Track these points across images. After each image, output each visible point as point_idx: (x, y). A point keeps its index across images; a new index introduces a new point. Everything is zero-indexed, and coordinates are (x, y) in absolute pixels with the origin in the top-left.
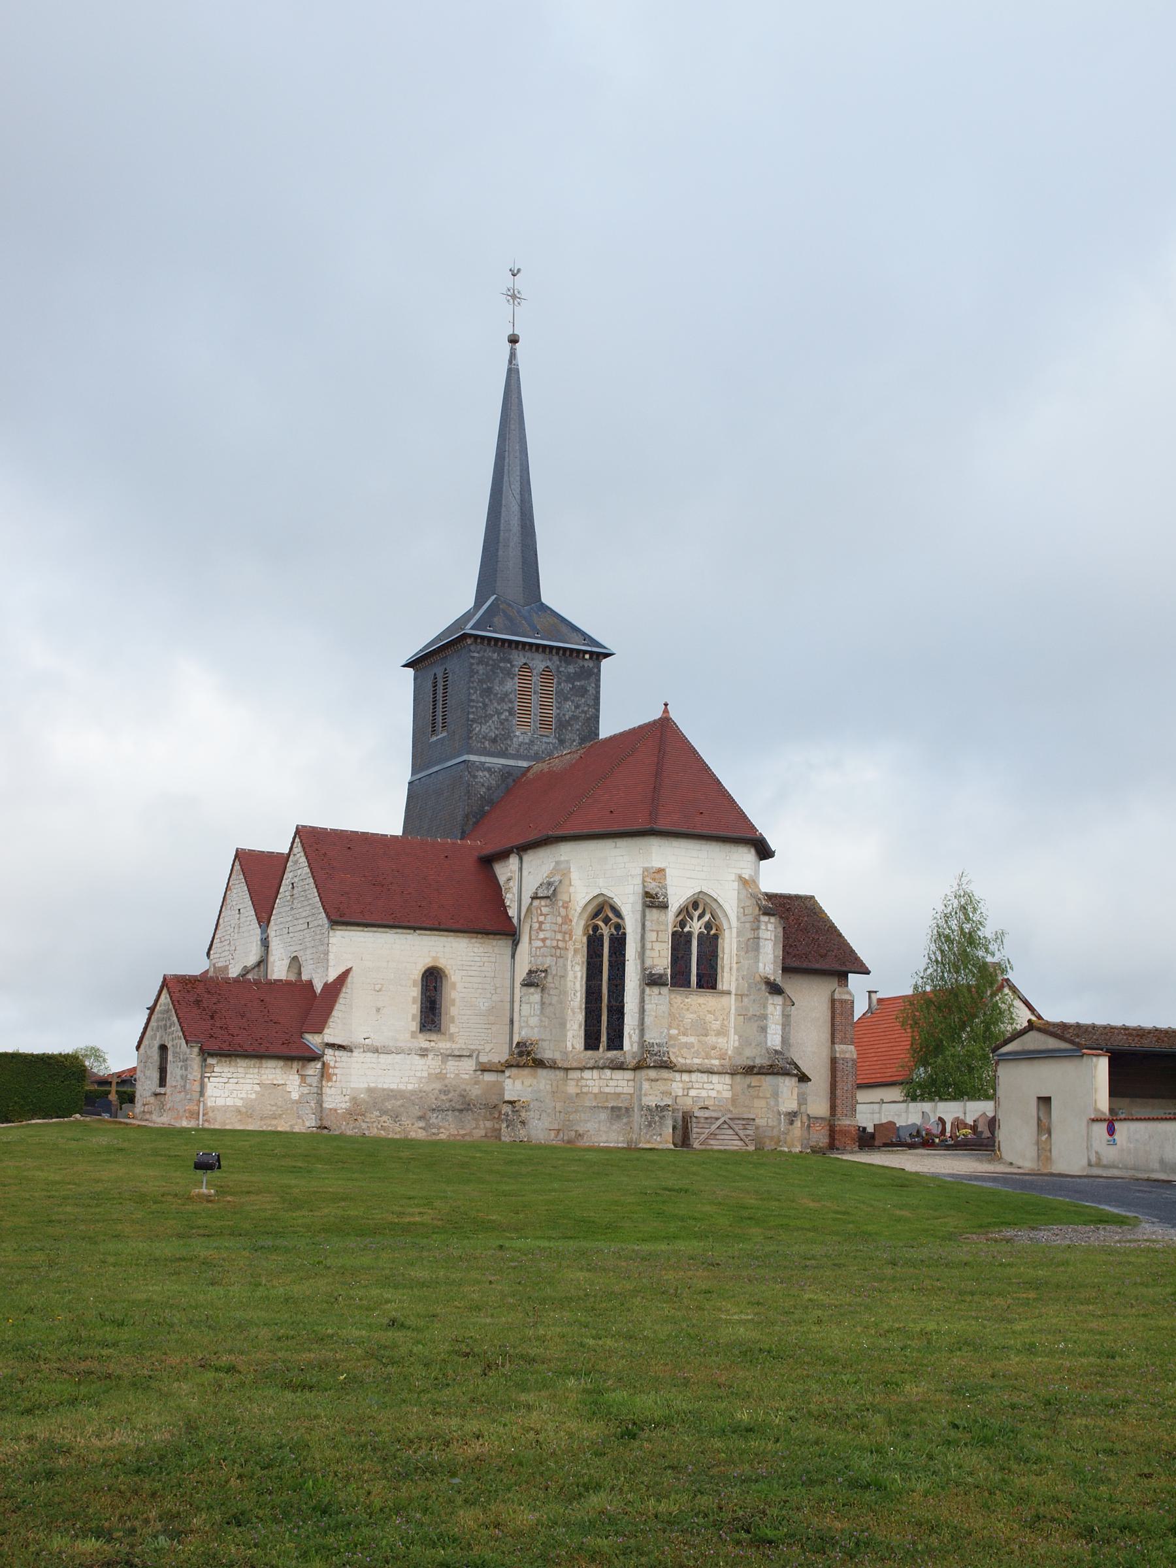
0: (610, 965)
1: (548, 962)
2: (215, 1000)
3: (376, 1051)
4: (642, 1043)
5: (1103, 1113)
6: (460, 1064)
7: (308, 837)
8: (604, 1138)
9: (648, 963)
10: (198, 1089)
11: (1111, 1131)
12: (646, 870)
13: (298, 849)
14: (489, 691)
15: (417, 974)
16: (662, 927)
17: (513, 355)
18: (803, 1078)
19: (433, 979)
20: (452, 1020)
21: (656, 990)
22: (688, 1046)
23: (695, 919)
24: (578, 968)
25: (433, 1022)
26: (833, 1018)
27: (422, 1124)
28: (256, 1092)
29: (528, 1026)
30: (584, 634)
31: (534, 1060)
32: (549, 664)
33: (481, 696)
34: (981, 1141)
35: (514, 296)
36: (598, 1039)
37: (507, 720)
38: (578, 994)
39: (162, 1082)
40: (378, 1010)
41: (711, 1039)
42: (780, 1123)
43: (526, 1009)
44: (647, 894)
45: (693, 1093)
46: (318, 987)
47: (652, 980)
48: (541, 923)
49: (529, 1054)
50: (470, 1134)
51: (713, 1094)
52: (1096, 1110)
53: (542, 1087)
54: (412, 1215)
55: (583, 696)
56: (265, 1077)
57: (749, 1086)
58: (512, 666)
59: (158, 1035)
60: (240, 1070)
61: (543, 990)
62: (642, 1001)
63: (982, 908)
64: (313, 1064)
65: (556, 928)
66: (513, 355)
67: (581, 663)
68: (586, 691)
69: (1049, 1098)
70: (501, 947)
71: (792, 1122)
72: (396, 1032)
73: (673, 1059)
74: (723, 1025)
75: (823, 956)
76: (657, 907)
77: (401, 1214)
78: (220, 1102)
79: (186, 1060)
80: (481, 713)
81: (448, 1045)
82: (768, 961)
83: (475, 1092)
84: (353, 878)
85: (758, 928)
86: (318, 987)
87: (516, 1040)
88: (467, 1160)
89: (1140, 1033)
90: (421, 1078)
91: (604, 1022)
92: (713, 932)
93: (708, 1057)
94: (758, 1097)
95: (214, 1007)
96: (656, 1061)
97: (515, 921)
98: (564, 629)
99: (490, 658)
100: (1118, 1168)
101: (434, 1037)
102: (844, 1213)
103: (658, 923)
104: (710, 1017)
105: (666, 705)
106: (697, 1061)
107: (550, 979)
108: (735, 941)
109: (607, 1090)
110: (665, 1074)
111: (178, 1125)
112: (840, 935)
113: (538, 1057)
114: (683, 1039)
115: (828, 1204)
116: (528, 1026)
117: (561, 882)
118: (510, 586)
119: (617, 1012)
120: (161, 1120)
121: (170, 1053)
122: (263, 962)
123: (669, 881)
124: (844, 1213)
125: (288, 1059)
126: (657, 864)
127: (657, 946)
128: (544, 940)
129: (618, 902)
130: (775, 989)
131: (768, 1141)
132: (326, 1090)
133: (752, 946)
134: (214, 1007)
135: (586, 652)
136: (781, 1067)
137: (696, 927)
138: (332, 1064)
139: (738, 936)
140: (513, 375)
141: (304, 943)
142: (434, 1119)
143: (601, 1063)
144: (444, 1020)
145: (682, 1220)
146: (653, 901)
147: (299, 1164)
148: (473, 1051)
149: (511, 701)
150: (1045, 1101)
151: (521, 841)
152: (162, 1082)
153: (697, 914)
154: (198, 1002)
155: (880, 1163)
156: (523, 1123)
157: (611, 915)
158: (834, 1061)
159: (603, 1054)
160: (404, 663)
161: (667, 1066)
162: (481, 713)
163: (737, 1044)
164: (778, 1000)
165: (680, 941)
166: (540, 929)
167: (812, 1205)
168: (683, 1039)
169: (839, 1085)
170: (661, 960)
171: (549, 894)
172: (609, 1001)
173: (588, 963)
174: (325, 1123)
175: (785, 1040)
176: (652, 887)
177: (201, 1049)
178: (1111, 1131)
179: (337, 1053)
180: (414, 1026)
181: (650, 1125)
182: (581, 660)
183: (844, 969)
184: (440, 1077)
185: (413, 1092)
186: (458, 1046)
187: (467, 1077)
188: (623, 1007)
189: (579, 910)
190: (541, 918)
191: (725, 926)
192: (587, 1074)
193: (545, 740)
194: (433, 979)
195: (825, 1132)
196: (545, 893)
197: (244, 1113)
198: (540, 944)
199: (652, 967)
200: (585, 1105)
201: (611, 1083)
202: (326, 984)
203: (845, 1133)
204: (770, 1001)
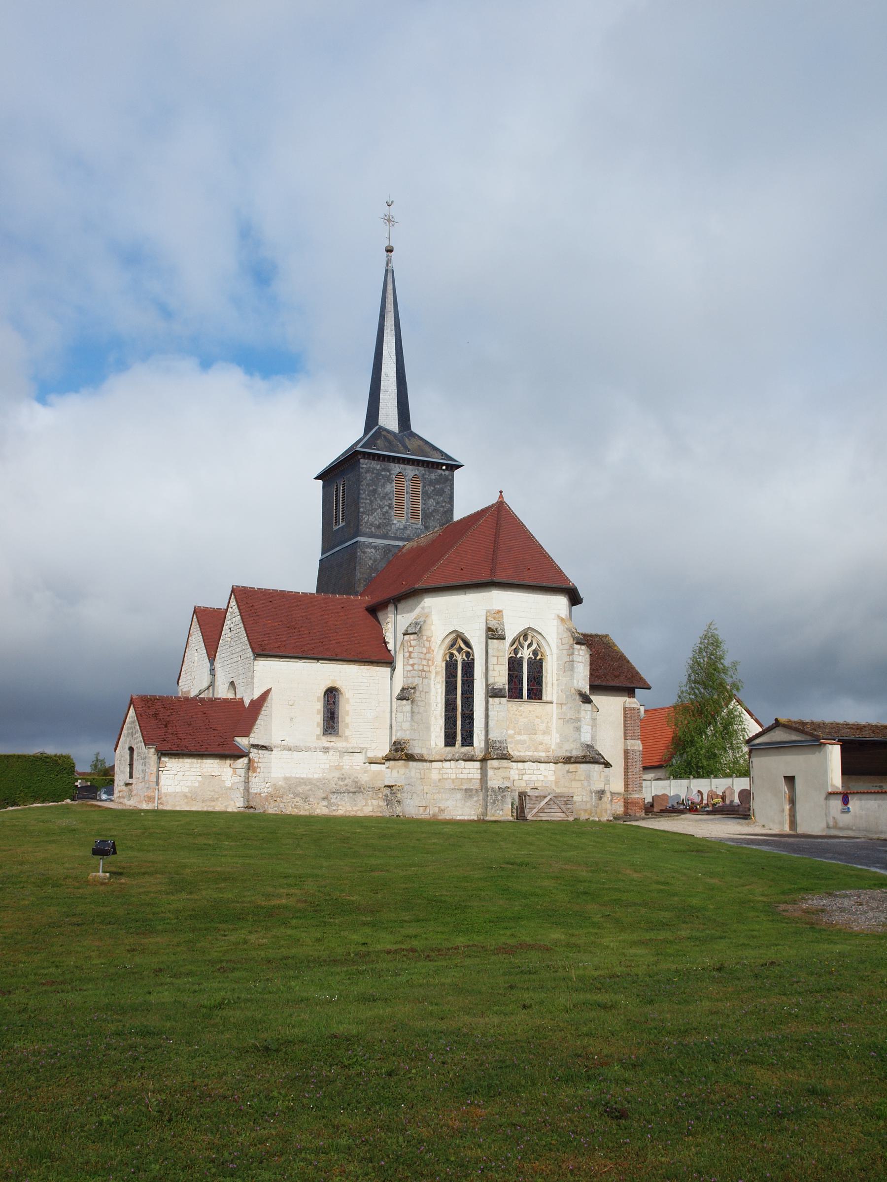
0: (463, 684)
1: (417, 681)
2: (169, 713)
3: (290, 750)
4: (487, 740)
5: (837, 788)
6: (353, 758)
7: (244, 596)
8: (460, 812)
9: (491, 681)
10: (155, 780)
11: (846, 802)
12: (488, 611)
13: (233, 603)
14: (375, 491)
15: (321, 692)
16: (501, 654)
17: (389, 261)
18: (607, 765)
19: (332, 695)
20: (347, 726)
21: (497, 700)
22: (523, 742)
23: (526, 647)
24: (438, 686)
25: (333, 728)
26: (625, 721)
27: (325, 803)
28: (199, 782)
29: (402, 729)
30: (441, 452)
31: (406, 755)
32: (417, 472)
33: (369, 495)
34: (740, 810)
35: (389, 220)
36: (455, 738)
37: (387, 512)
38: (439, 705)
39: (131, 777)
40: (291, 719)
41: (539, 737)
42: (592, 799)
43: (400, 715)
44: (489, 629)
45: (526, 777)
46: (247, 703)
47: (493, 693)
48: (410, 653)
49: (402, 750)
50: (361, 810)
51: (541, 778)
52: (833, 786)
53: (413, 774)
54: (280, 896)
55: (441, 495)
56: (205, 770)
57: (568, 772)
58: (391, 474)
59: (128, 740)
60: (186, 765)
61: (412, 702)
62: (487, 709)
63: (724, 647)
64: (241, 760)
65: (422, 656)
66: (389, 261)
67: (440, 472)
68: (444, 492)
69: (794, 777)
70: (383, 672)
71: (600, 798)
72: (324, 744)
73: (510, 752)
74: (547, 727)
75: (617, 677)
76: (497, 639)
77: (268, 896)
78: (171, 790)
79: (145, 758)
80: (369, 507)
81: (344, 744)
82: (582, 678)
83: (364, 779)
84: (276, 624)
85: (573, 654)
86: (247, 703)
87: (394, 740)
88: (349, 835)
89: (859, 728)
90: (324, 769)
91: (459, 726)
92: (538, 658)
93: (536, 750)
94: (575, 780)
95: (168, 718)
96: (496, 753)
97: (392, 652)
98: (427, 449)
99: (374, 469)
100: (851, 829)
101: (333, 739)
102: (663, 883)
103: (498, 650)
104: (537, 721)
105: (501, 492)
106: (530, 754)
107: (417, 694)
108: (555, 664)
109: (461, 776)
110: (504, 763)
111: (140, 807)
112: (628, 662)
113: (410, 752)
114: (518, 737)
115: (649, 875)
116: (402, 729)
117: (425, 621)
118: (389, 419)
119: (468, 718)
120: (130, 803)
121: (135, 753)
122: (212, 684)
123: (505, 620)
124: (663, 883)
125: (223, 757)
126: (496, 607)
127: (497, 668)
128: (413, 665)
129: (468, 636)
130: (586, 700)
131: (583, 813)
132: (252, 779)
133: (569, 666)
134: (168, 718)
135: (443, 464)
136: (592, 757)
137: (526, 654)
138: (256, 760)
139: (558, 660)
140: (389, 273)
141: (237, 672)
142: (334, 798)
143: (456, 757)
144: (341, 725)
145: (525, 897)
146: (493, 634)
147: (211, 842)
148: (363, 749)
149: (390, 499)
150: (790, 780)
151: (395, 593)
152: (131, 777)
153: (526, 644)
154: (156, 715)
155: (662, 828)
156: (399, 802)
157: (463, 646)
158: (626, 752)
159: (458, 749)
160: (315, 476)
161: (506, 757)
162: (369, 507)
163: (558, 740)
164: (588, 706)
165: (514, 665)
166: (410, 657)
167: (635, 875)
168: (518, 737)
169: (631, 769)
170: (500, 677)
171: (416, 631)
172: (462, 710)
173: (447, 682)
174: (252, 804)
175: (593, 738)
176: (493, 624)
177: (157, 750)
178: (846, 802)
179: (260, 751)
180: (319, 730)
181: (494, 802)
182: (440, 469)
183: (632, 685)
184: (338, 768)
185: (319, 780)
186: (351, 745)
187: (358, 768)
188: (473, 714)
189: (439, 642)
190: (411, 649)
191: (548, 652)
192: (447, 764)
193: (415, 526)
194: (332, 695)
195: (621, 803)
196: (413, 631)
197: (191, 797)
198: (410, 668)
199: (494, 684)
200: (445, 791)
201: (465, 771)
202: (252, 701)
203: (635, 803)
204: (583, 708)
